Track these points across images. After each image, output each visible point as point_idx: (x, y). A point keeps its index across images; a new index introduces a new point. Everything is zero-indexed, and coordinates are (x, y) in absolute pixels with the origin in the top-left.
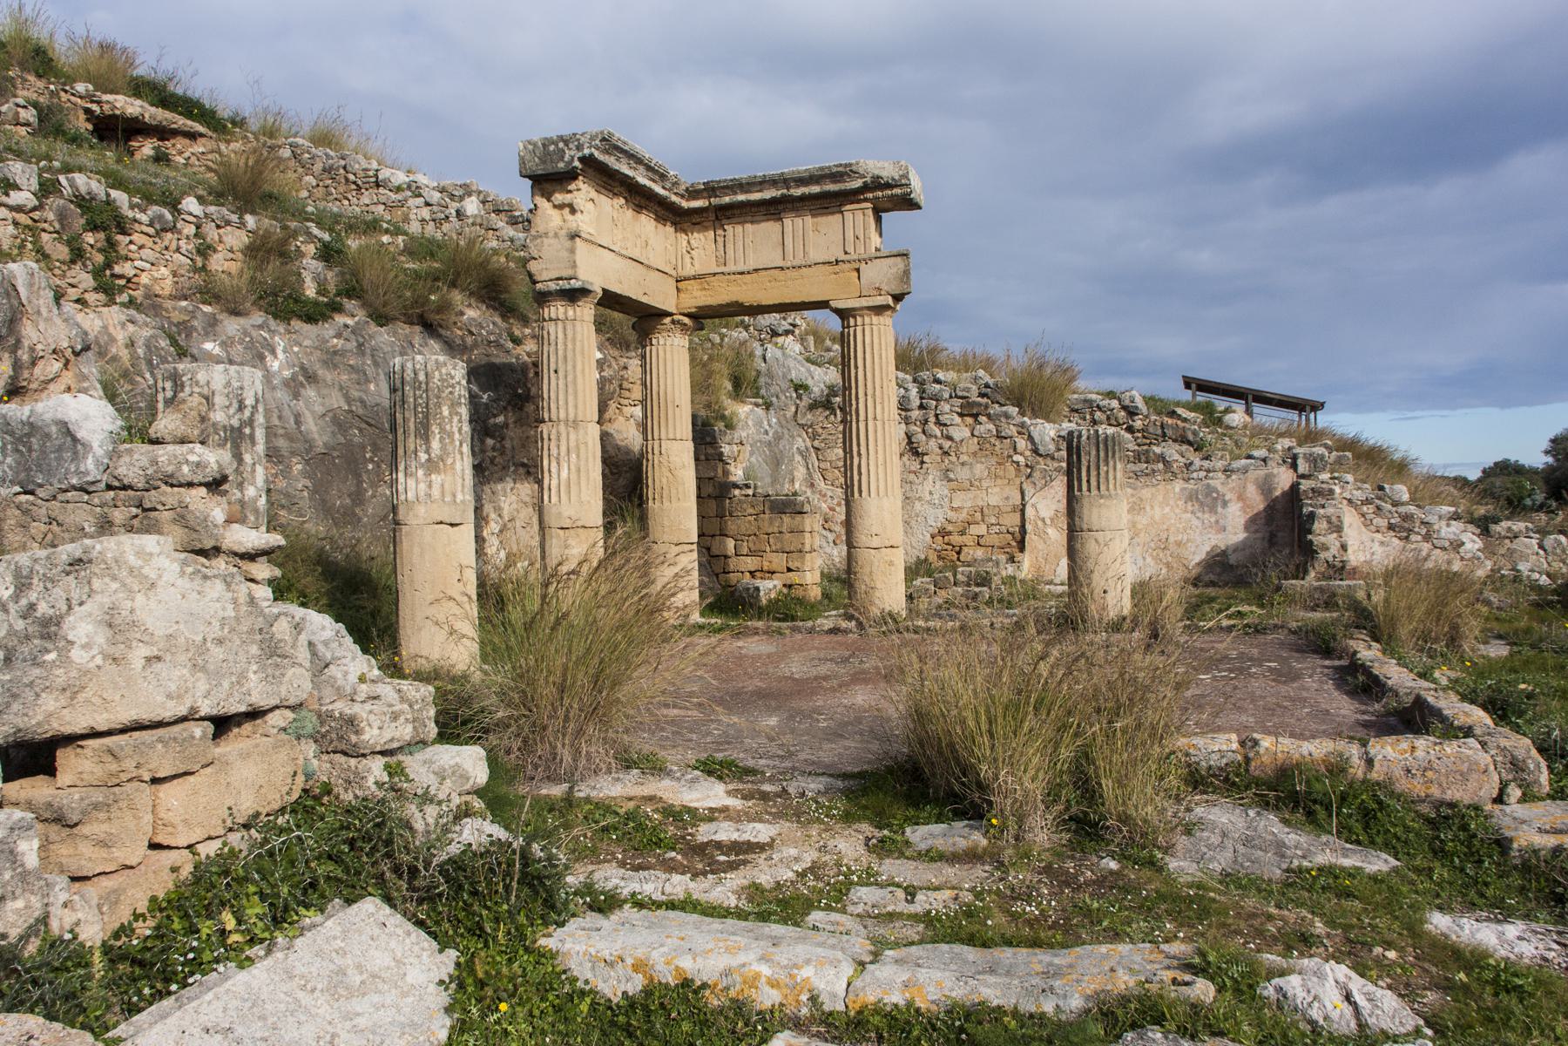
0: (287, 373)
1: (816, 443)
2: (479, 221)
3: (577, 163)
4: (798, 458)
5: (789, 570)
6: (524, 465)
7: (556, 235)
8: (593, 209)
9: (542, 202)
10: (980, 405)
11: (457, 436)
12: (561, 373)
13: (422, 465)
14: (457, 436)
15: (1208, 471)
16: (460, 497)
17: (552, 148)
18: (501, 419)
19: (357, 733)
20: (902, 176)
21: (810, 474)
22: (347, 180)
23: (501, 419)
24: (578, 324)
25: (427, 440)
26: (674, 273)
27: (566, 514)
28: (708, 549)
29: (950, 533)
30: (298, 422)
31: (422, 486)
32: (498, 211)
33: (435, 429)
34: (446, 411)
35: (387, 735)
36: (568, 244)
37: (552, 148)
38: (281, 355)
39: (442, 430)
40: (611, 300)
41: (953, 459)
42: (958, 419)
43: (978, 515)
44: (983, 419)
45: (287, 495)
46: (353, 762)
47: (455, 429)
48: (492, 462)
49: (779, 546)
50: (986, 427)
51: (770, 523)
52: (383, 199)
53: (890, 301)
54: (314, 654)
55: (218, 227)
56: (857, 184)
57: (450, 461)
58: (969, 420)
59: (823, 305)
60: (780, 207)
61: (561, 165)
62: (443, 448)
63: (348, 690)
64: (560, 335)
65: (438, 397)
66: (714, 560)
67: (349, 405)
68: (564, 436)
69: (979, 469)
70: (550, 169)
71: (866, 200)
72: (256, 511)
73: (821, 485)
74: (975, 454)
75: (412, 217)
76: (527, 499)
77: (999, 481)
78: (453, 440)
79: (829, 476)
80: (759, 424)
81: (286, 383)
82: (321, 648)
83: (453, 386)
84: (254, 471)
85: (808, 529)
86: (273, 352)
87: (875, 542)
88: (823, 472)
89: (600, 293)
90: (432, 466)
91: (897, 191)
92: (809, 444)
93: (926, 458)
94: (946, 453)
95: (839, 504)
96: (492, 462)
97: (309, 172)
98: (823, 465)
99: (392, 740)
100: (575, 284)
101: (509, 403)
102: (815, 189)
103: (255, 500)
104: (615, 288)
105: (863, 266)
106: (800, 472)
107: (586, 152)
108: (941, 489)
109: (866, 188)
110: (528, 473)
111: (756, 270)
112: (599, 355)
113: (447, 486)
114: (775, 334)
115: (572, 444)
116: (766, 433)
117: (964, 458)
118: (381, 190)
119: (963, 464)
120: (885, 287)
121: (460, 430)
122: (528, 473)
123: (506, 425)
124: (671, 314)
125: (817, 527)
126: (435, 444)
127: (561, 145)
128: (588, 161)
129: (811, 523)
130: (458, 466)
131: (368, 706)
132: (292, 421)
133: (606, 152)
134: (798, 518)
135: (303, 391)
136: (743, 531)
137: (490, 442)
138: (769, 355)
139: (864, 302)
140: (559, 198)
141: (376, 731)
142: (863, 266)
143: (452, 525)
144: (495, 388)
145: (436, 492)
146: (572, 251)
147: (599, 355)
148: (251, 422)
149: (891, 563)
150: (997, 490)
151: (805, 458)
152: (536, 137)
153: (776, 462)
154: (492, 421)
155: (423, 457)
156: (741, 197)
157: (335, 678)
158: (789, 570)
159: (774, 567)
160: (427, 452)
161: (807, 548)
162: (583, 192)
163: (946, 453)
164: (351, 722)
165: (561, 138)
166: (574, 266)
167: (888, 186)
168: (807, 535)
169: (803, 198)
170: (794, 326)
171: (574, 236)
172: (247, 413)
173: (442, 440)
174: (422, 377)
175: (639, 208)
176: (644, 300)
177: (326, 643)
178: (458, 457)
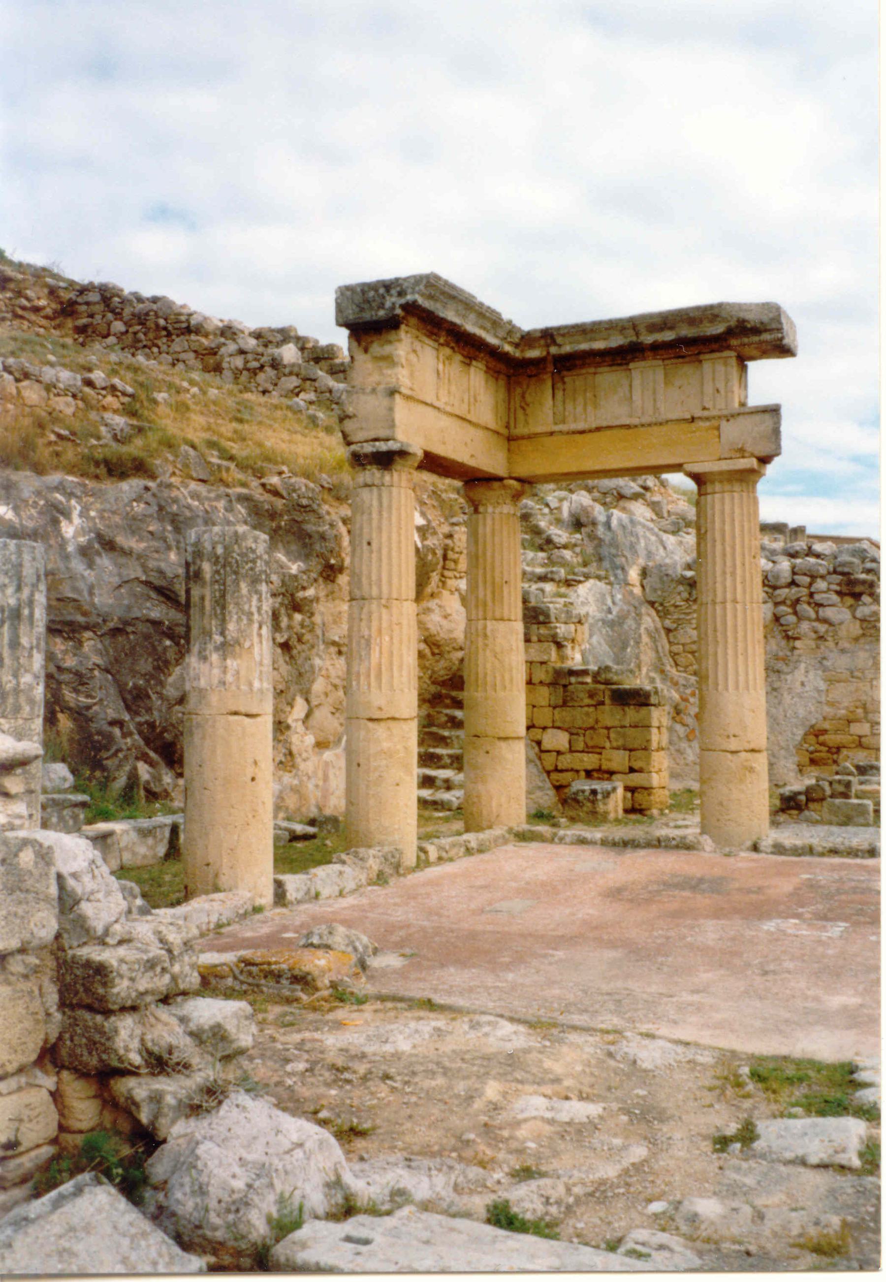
0: (82, 540)
1: (668, 623)
2: (296, 370)
3: (398, 311)
4: (645, 639)
5: (632, 770)
7: (374, 391)
8: (414, 361)
9: (360, 357)
10: (864, 582)
12: (374, 545)
13: (217, 649)
14: (256, 617)
16: (257, 684)
17: (372, 293)
19: (105, 985)
20: (772, 319)
21: (659, 659)
22: (157, 325)
24: (395, 490)
25: (223, 621)
28: (539, 743)
29: (825, 732)
30: (91, 594)
31: (216, 671)
32: (317, 360)
33: (231, 607)
34: (244, 587)
36: (385, 402)
38: (77, 520)
40: (433, 463)
41: (831, 644)
42: (835, 598)
43: (860, 711)
45: (78, 674)
46: (99, 1018)
47: (254, 609)
48: (300, 640)
49: (620, 743)
51: (610, 715)
52: (194, 346)
53: (754, 463)
54: (62, 886)
55: (17, 380)
56: (719, 329)
58: (849, 601)
61: (382, 313)
63: (100, 931)
64: (375, 503)
65: (236, 573)
66: (544, 756)
67: (147, 576)
68: (375, 616)
70: (367, 316)
71: (729, 348)
72: (31, 702)
73: (673, 671)
74: (856, 639)
75: (225, 365)
76: (337, 681)
78: (250, 621)
79: (681, 660)
80: (602, 600)
81: (85, 552)
82: (71, 883)
83: (254, 561)
84: (31, 656)
85: (655, 723)
86: (67, 515)
87: (733, 745)
88: (674, 655)
89: (420, 454)
91: (766, 337)
92: (659, 625)
93: (798, 644)
94: (821, 638)
95: (693, 694)
96: (300, 640)
97: (118, 315)
98: (675, 649)
100: (393, 446)
101: (321, 574)
102: (668, 336)
103: (31, 688)
106: (648, 657)
107: (409, 298)
108: (816, 680)
109: (730, 332)
110: (340, 653)
111: (598, 429)
113: (243, 673)
114: (621, 497)
115: (385, 625)
116: (609, 611)
117: (845, 644)
118: (193, 337)
119: (843, 651)
120: (749, 448)
121: (259, 609)
122: (340, 653)
123: (317, 599)
124: (500, 479)
125: (666, 721)
126: (231, 627)
127: (382, 291)
128: (411, 309)
129: (659, 716)
130: (256, 649)
131: (122, 951)
132: (86, 593)
133: (431, 297)
134: (644, 710)
135: (98, 560)
136: (579, 723)
137: (298, 617)
138: (614, 523)
139: (725, 466)
140: (376, 349)
141: (126, 983)
142: (724, 424)
143: (247, 715)
144: (307, 557)
146: (391, 409)
148: (31, 603)
149: (751, 770)
151: (654, 640)
153: (620, 644)
154: (300, 594)
156: (584, 346)
159: (614, 766)
160: (222, 634)
161: (654, 745)
163: (821, 638)
164: (100, 971)
166: (392, 425)
168: (654, 731)
169: (656, 348)
170: (646, 488)
171: (392, 392)
172: (26, 592)
173: (239, 619)
176: (472, 463)
177: (74, 875)
178: (256, 639)
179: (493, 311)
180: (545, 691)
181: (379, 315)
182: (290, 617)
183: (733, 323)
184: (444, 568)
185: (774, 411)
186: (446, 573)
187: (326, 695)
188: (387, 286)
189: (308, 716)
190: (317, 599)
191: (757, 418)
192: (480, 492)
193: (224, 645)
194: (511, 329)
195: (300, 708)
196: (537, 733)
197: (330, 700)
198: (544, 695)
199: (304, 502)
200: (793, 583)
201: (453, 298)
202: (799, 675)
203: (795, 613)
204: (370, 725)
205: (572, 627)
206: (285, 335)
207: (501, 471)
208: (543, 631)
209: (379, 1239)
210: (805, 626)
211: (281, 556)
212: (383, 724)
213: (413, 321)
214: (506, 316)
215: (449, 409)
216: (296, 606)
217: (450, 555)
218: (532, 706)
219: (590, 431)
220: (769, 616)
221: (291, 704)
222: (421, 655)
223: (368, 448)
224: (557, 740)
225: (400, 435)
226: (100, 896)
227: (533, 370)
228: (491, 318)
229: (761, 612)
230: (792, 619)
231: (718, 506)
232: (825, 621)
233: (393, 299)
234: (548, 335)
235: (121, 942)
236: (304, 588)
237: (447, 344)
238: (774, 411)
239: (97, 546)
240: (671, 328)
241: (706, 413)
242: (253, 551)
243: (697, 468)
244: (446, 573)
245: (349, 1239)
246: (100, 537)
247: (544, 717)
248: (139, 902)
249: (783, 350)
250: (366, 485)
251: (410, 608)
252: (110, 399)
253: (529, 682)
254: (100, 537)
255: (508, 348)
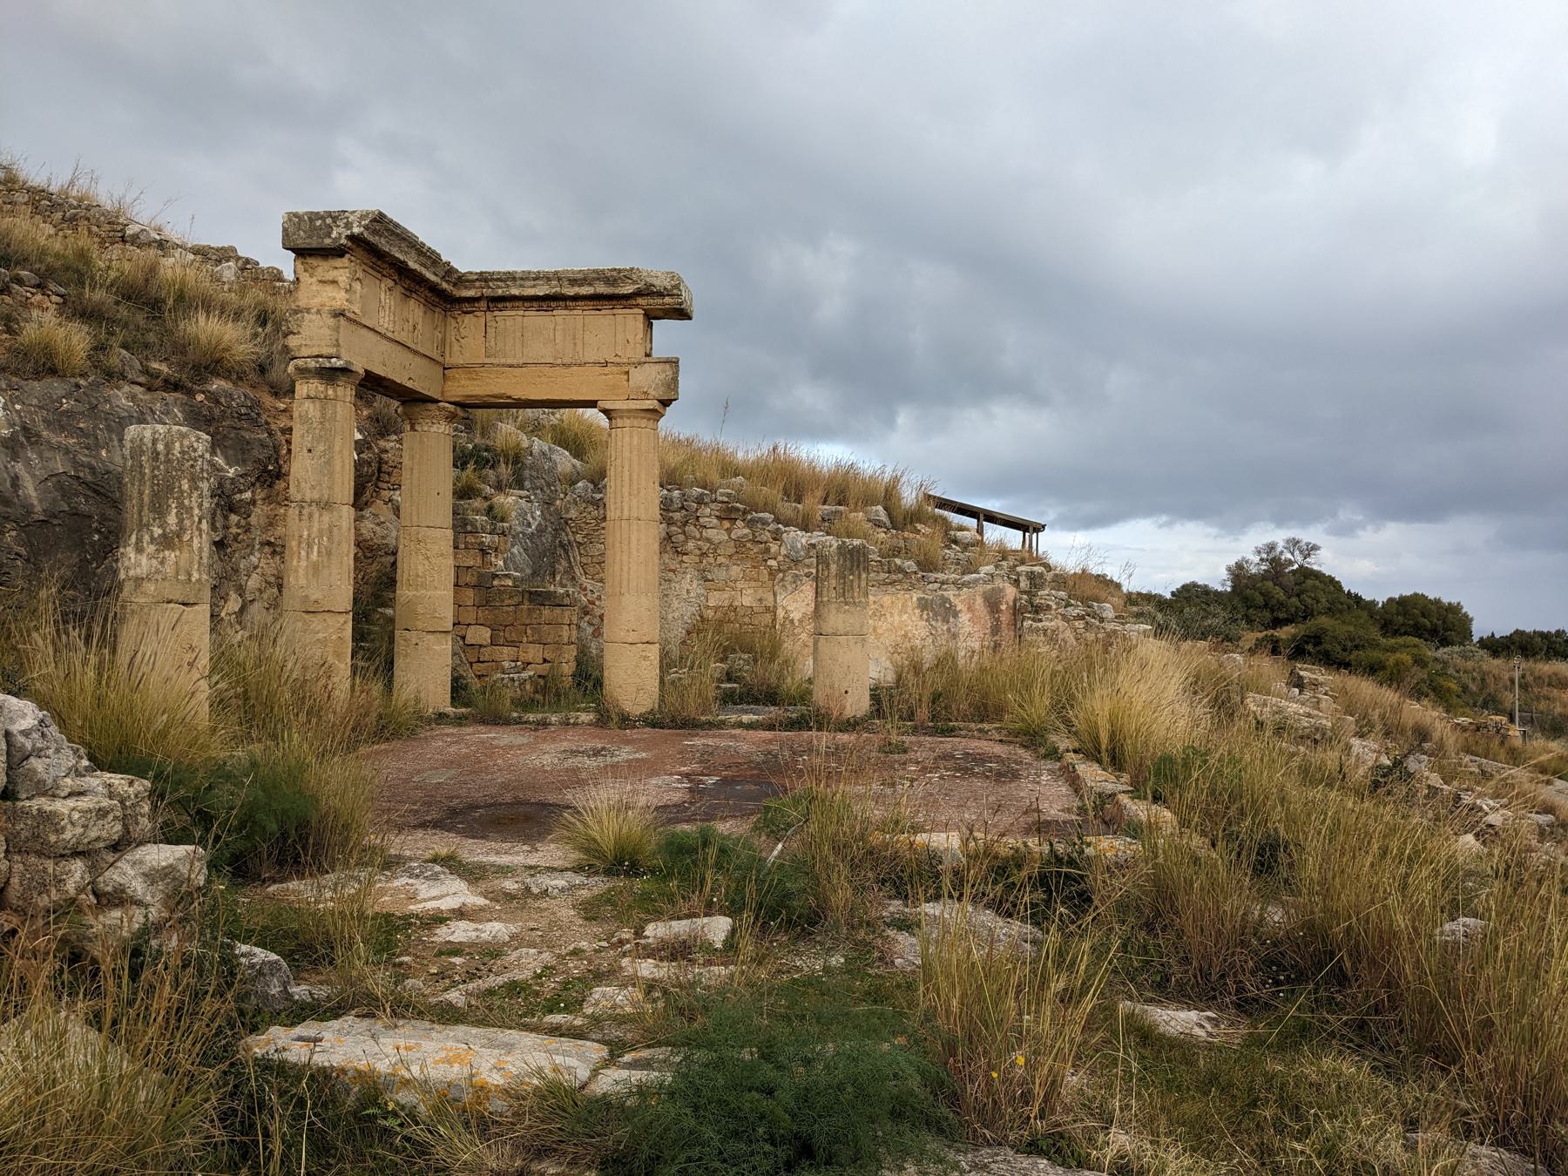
5: (545, 661)
6: (269, 543)
7: (318, 312)
9: (305, 277)
11: (196, 511)
14: (196, 511)
15: (943, 583)
16: (195, 576)
17: (318, 223)
18: (248, 495)
23: (248, 495)
26: (440, 359)
27: (313, 598)
28: (463, 638)
35: (93, 834)
37: (318, 223)
39: (181, 506)
44: (739, 523)
47: (194, 504)
50: (741, 530)
56: (628, 289)
57: (186, 538)
58: (727, 524)
59: (592, 404)
60: (553, 304)
61: (327, 241)
62: (181, 521)
66: (469, 649)
67: (76, 470)
69: (735, 571)
77: (753, 584)
79: (591, 570)
88: (583, 565)
89: (361, 371)
90: (167, 542)
91: (667, 300)
99: (98, 839)
100: (339, 363)
102: (586, 290)
104: (379, 370)
105: (632, 370)
107: (356, 230)
109: (638, 294)
110: (274, 553)
112: (358, 436)
116: (529, 525)
117: (721, 560)
120: (652, 392)
122: (274, 553)
123: (253, 502)
126: (172, 519)
127: (329, 221)
130: (196, 541)
131: (71, 803)
137: (234, 518)
142: (632, 370)
145: (169, 569)
146: (337, 329)
147: (358, 436)
150: (750, 591)
152: (301, 209)
154: (238, 497)
155: (157, 531)
157: (35, 771)
158: (545, 661)
162: (341, 271)
163: (704, 555)
165: (329, 214)
167: (661, 295)
169: (576, 298)
174: (160, 447)
175: (408, 293)
176: (409, 384)
179: (434, 252)
180: (470, 593)
181: (313, 242)
182: (226, 518)
183: (641, 285)
184: (378, 479)
185: (674, 363)
186: (381, 485)
187: (261, 591)
188: (335, 217)
189: (243, 609)
190: (253, 502)
191: (659, 367)
192: (417, 409)
193: (164, 535)
194: (449, 271)
195: (234, 604)
196: (461, 630)
197: (265, 596)
198: (469, 596)
199: (243, 411)
200: (683, 507)
201: (393, 233)
202: (685, 584)
203: (684, 533)
204: (306, 616)
205: (496, 538)
206: (226, 254)
207: (436, 396)
208: (471, 539)
209: (327, 1035)
210: (691, 545)
211: (220, 460)
212: (320, 616)
213: (360, 252)
214: (444, 259)
215: (389, 335)
216: (232, 509)
217: (385, 467)
218: (458, 605)
219: (519, 366)
220: (664, 534)
221: (225, 598)
222: (356, 558)
223: (312, 364)
224: (480, 635)
225: (346, 356)
226: (50, 752)
227: (466, 306)
228: (432, 258)
229: (651, 496)
230: (681, 537)
231: (627, 439)
232: (708, 540)
233: (341, 230)
234: (484, 278)
235: (70, 795)
236: (241, 492)
237: (390, 276)
238: (674, 363)
239: (22, 439)
240: (590, 285)
241: (617, 360)
242: (195, 450)
243: (608, 406)
244: (381, 485)
245: (300, 1039)
246: (25, 428)
247: (470, 616)
248: (85, 762)
249: (682, 314)
250: (309, 397)
251: (348, 513)
252: (39, 297)
253: (456, 585)
254: (25, 428)
255: (445, 285)
